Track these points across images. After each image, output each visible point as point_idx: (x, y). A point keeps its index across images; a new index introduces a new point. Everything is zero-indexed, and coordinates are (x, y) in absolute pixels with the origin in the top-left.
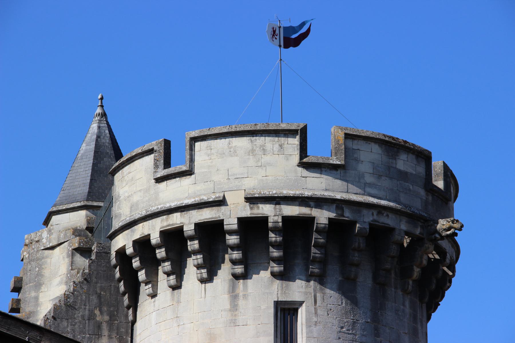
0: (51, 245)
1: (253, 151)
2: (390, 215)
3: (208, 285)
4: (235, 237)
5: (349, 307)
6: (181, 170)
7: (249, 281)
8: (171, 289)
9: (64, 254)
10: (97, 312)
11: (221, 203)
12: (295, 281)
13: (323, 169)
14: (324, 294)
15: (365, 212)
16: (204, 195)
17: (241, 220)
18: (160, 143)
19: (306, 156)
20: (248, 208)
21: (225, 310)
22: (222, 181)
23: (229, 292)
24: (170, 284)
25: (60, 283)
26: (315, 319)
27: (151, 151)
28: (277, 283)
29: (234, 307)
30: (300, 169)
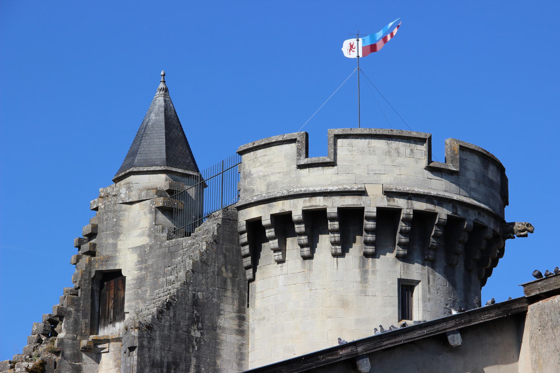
0: (130, 200)
1: (389, 152)
2: (485, 215)
3: (340, 259)
4: (372, 223)
5: (451, 288)
6: (325, 161)
7: (377, 260)
8: (302, 259)
9: (145, 210)
10: (223, 269)
11: (362, 193)
12: (414, 264)
13: (443, 174)
14: (435, 275)
15: (471, 212)
16: (347, 184)
17: (379, 209)
18: (302, 135)
19: (432, 162)
20: (386, 200)
21: (356, 282)
22: (363, 174)
23: (360, 267)
24: (303, 255)
25: (142, 235)
26: (428, 296)
27: (293, 141)
28: (400, 263)
29: (364, 280)
30: (427, 172)
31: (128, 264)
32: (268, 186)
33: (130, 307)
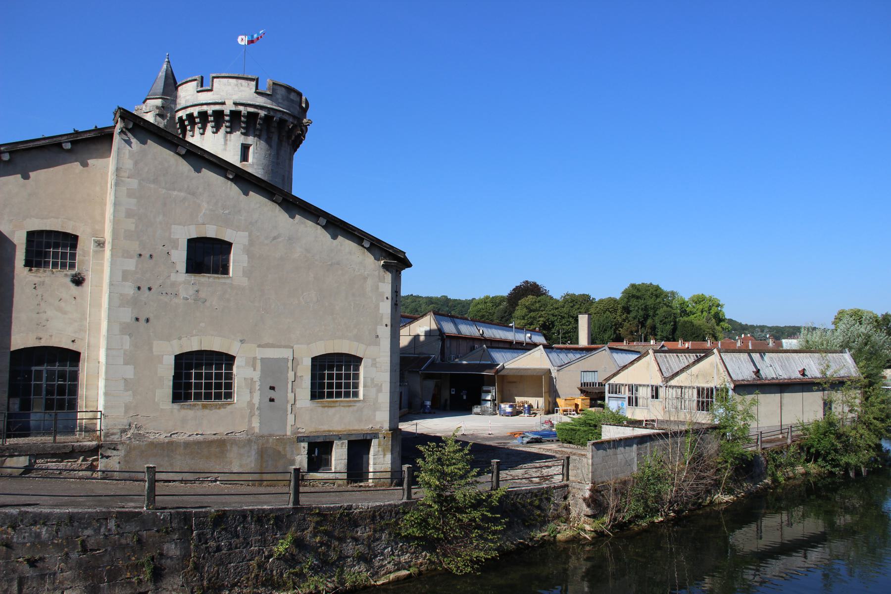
11: (224, 103)
17: (231, 111)
27: (195, 80)
29: (226, 144)
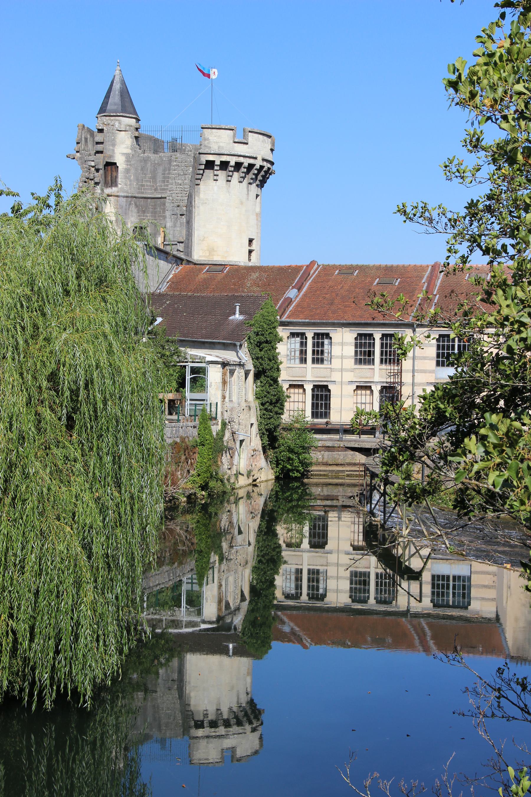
11: (256, 158)
31: (120, 161)
32: (219, 147)
33: (122, 181)
